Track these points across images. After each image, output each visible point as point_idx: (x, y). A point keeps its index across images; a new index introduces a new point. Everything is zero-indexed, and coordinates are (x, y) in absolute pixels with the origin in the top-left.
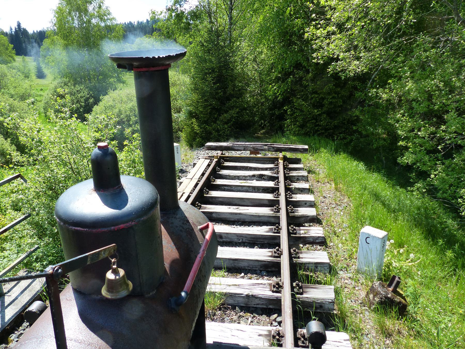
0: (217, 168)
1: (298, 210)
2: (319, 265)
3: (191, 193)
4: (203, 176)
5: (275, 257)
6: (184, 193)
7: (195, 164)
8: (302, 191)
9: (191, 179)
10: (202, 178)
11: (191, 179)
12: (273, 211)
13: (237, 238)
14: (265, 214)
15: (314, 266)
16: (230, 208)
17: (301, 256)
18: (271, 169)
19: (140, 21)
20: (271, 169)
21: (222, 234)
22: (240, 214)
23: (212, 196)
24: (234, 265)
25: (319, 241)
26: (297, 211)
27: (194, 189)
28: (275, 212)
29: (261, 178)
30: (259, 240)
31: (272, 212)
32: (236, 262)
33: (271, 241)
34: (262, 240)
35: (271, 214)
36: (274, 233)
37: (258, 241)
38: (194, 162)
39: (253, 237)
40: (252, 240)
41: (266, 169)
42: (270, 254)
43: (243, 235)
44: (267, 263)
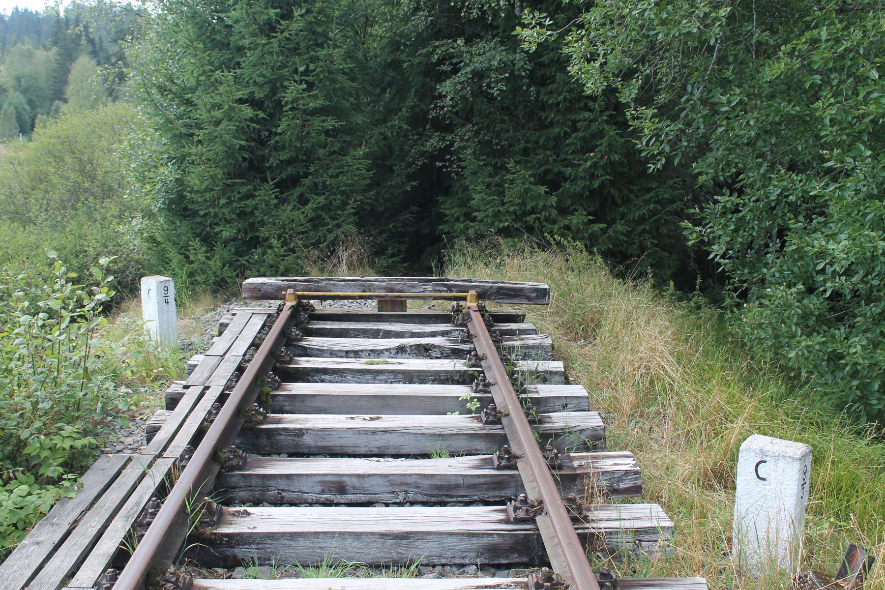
0: (295, 332)
1: (550, 417)
2: (646, 538)
3: (229, 387)
4: (121, 568)
5: (518, 521)
6: (207, 388)
7: (223, 327)
8: (545, 378)
9: (223, 356)
10: (157, 507)
11: (223, 356)
12: (481, 421)
13: (391, 489)
14: (458, 428)
15: (630, 538)
16: (352, 418)
17: (592, 515)
18: (444, 334)
19: (21, 8)
20: (444, 334)
21: (344, 479)
22: (385, 431)
23: (292, 393)
24: (398, 553)
25: (628, 485)
26: (549, 420)
27: (218, 409)
28: (487, 423)
29: (424, 351)
30: (453, 493)
31: (481, 425)
32: (404, 542)
33: (491, 493)
34: (462, 493)
35: (471, 429)
36: (499, 468)
37: (452, 497)
38: (222, 321)
39: (439, 483)
40: (436, 492)
41: (433, 334)
42: (502, 516)
43: (409, 480)
44: (496, 539)
